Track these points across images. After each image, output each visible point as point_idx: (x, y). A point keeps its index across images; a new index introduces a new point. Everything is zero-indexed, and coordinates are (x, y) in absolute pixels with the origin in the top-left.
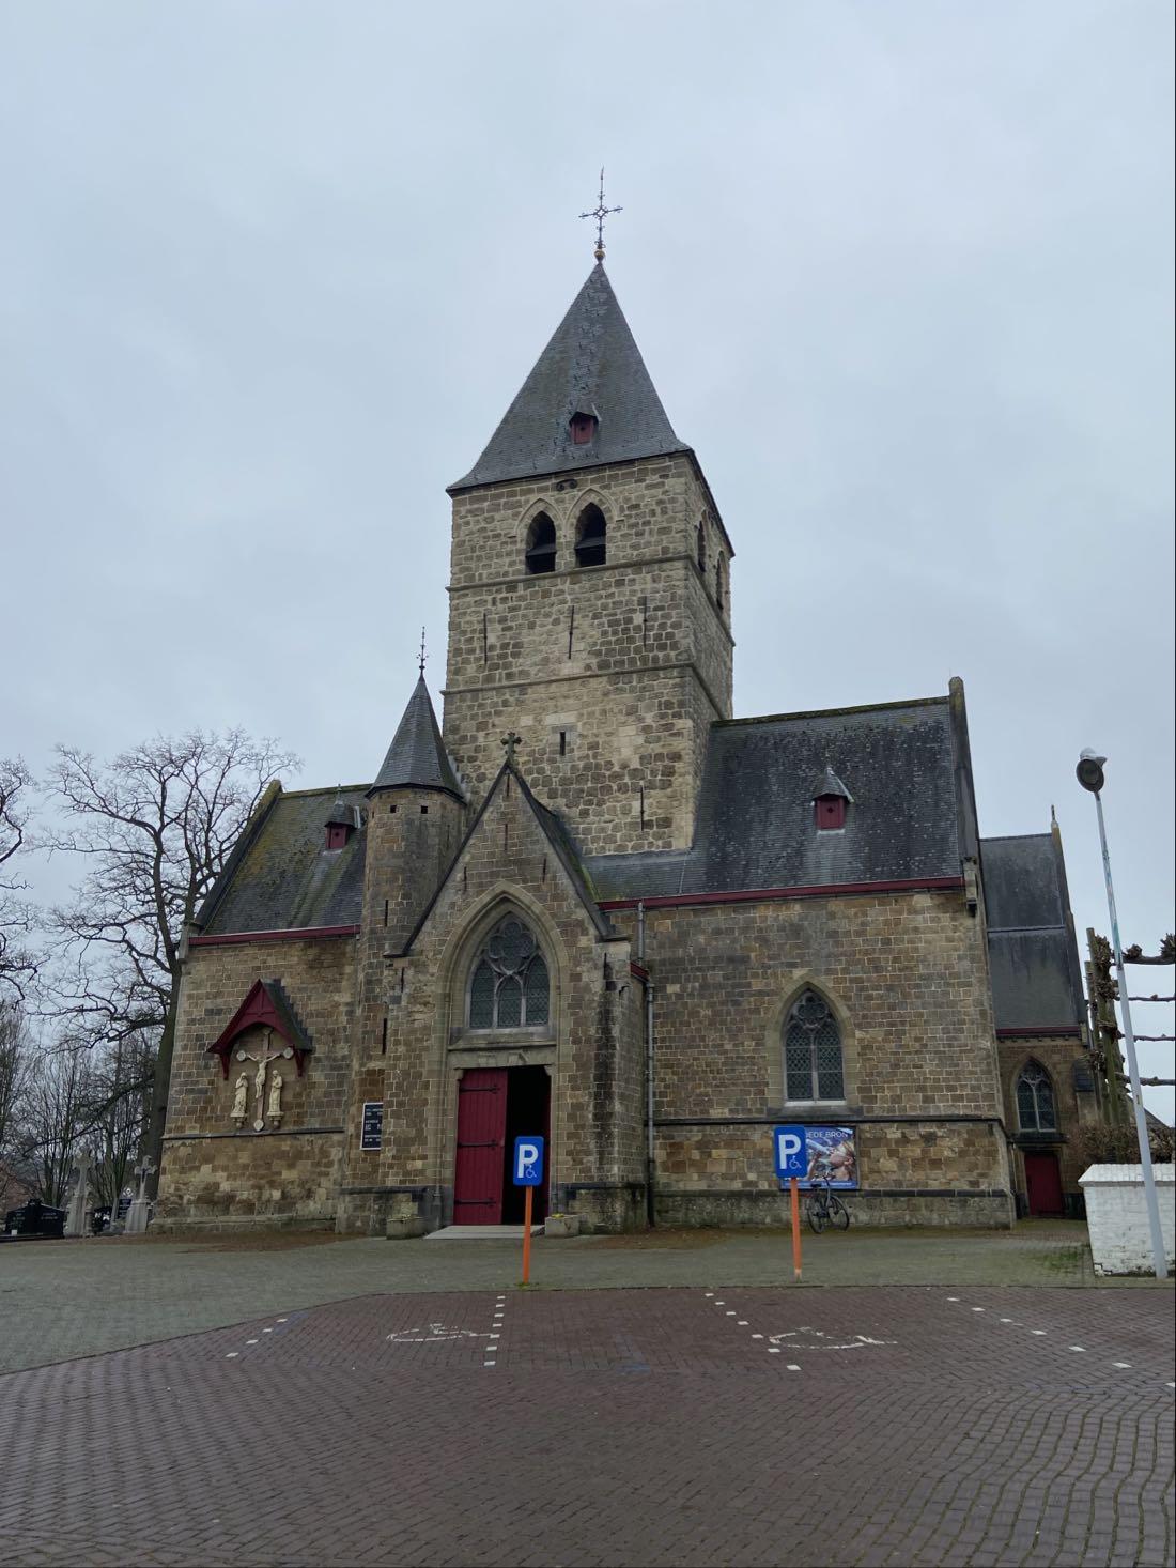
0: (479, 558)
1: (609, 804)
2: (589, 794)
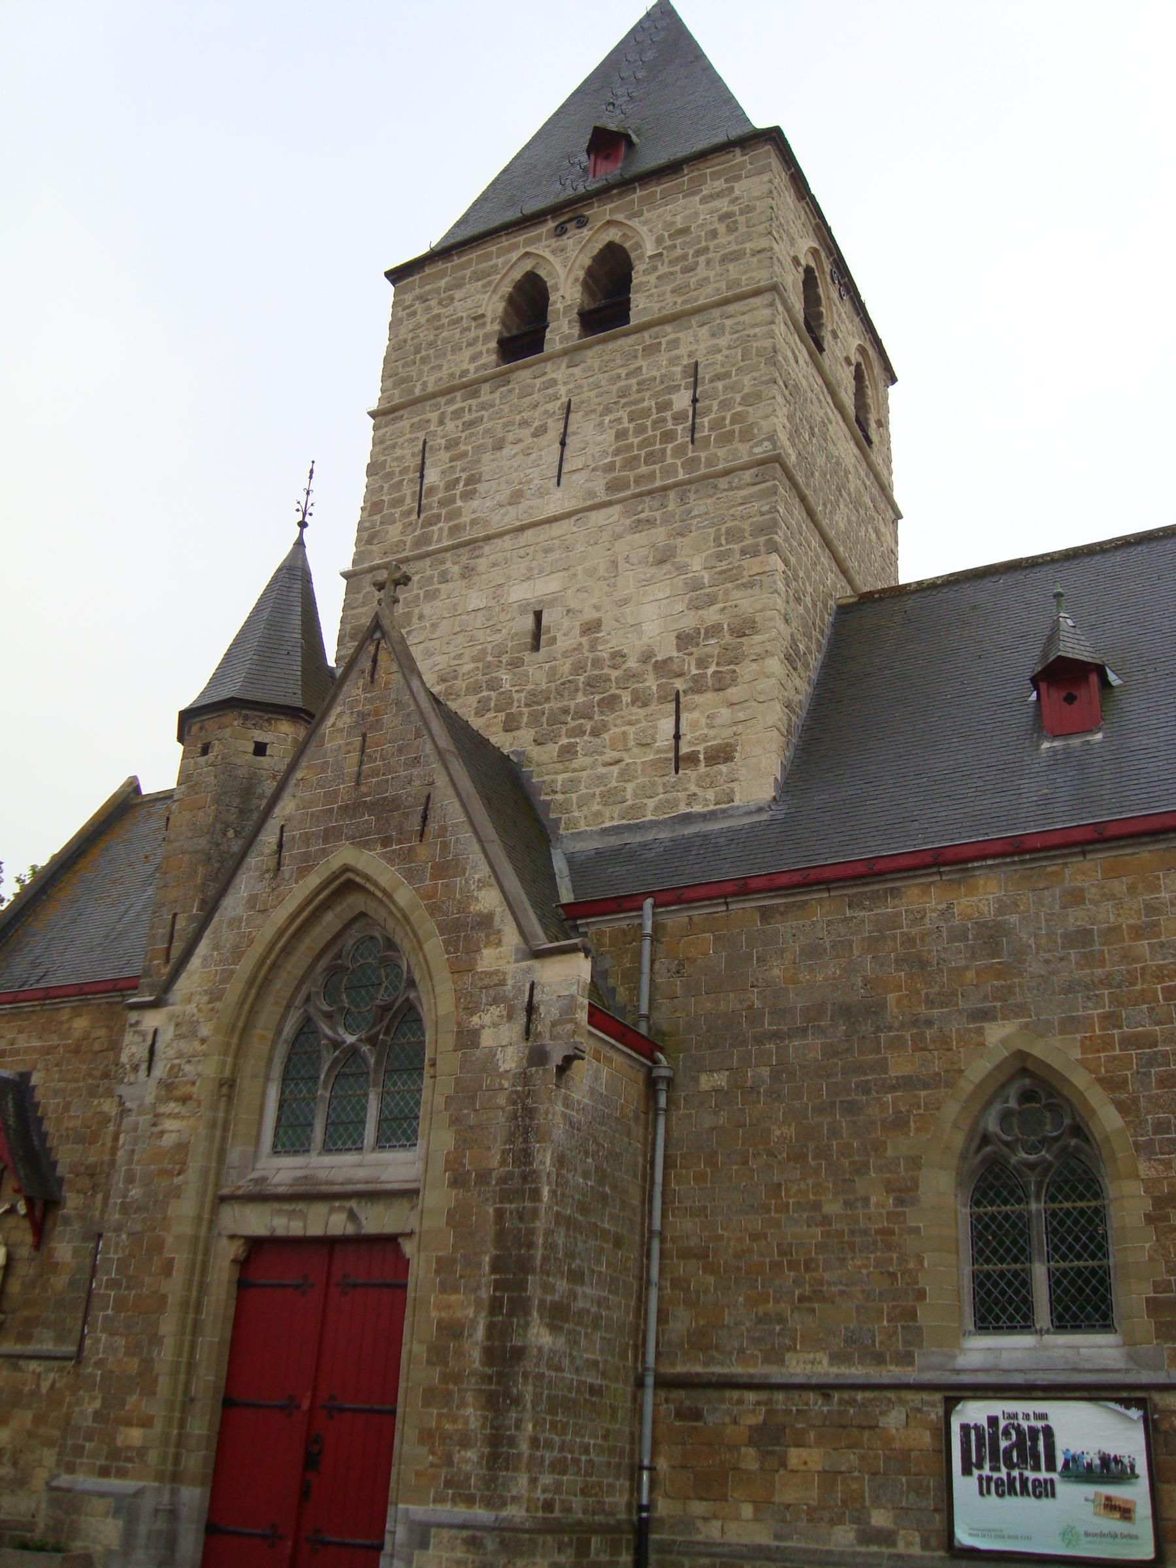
0: (424, 360)
1: (614, 730)
2: (578, 715)
